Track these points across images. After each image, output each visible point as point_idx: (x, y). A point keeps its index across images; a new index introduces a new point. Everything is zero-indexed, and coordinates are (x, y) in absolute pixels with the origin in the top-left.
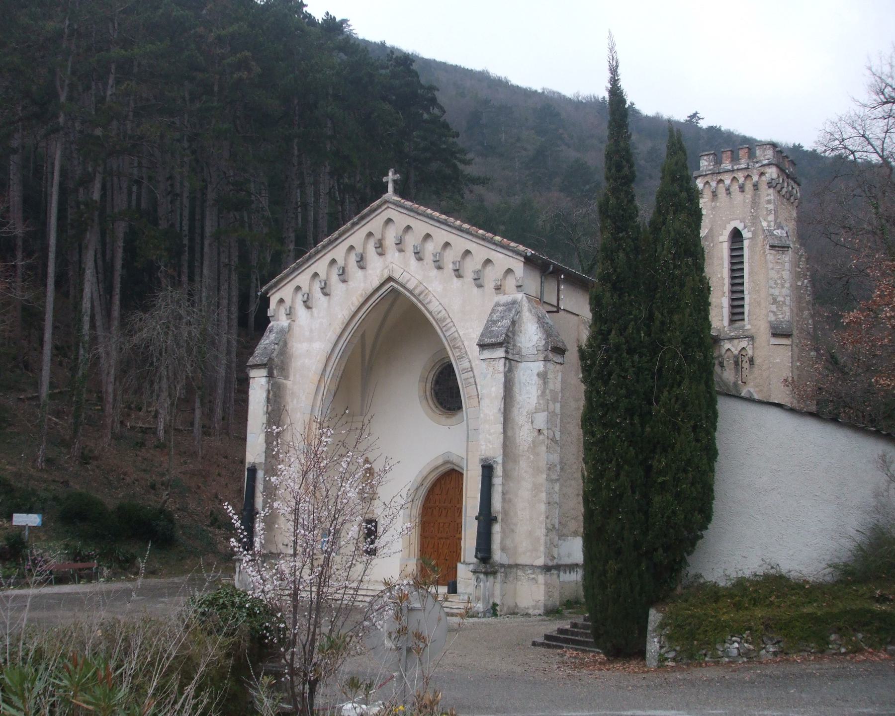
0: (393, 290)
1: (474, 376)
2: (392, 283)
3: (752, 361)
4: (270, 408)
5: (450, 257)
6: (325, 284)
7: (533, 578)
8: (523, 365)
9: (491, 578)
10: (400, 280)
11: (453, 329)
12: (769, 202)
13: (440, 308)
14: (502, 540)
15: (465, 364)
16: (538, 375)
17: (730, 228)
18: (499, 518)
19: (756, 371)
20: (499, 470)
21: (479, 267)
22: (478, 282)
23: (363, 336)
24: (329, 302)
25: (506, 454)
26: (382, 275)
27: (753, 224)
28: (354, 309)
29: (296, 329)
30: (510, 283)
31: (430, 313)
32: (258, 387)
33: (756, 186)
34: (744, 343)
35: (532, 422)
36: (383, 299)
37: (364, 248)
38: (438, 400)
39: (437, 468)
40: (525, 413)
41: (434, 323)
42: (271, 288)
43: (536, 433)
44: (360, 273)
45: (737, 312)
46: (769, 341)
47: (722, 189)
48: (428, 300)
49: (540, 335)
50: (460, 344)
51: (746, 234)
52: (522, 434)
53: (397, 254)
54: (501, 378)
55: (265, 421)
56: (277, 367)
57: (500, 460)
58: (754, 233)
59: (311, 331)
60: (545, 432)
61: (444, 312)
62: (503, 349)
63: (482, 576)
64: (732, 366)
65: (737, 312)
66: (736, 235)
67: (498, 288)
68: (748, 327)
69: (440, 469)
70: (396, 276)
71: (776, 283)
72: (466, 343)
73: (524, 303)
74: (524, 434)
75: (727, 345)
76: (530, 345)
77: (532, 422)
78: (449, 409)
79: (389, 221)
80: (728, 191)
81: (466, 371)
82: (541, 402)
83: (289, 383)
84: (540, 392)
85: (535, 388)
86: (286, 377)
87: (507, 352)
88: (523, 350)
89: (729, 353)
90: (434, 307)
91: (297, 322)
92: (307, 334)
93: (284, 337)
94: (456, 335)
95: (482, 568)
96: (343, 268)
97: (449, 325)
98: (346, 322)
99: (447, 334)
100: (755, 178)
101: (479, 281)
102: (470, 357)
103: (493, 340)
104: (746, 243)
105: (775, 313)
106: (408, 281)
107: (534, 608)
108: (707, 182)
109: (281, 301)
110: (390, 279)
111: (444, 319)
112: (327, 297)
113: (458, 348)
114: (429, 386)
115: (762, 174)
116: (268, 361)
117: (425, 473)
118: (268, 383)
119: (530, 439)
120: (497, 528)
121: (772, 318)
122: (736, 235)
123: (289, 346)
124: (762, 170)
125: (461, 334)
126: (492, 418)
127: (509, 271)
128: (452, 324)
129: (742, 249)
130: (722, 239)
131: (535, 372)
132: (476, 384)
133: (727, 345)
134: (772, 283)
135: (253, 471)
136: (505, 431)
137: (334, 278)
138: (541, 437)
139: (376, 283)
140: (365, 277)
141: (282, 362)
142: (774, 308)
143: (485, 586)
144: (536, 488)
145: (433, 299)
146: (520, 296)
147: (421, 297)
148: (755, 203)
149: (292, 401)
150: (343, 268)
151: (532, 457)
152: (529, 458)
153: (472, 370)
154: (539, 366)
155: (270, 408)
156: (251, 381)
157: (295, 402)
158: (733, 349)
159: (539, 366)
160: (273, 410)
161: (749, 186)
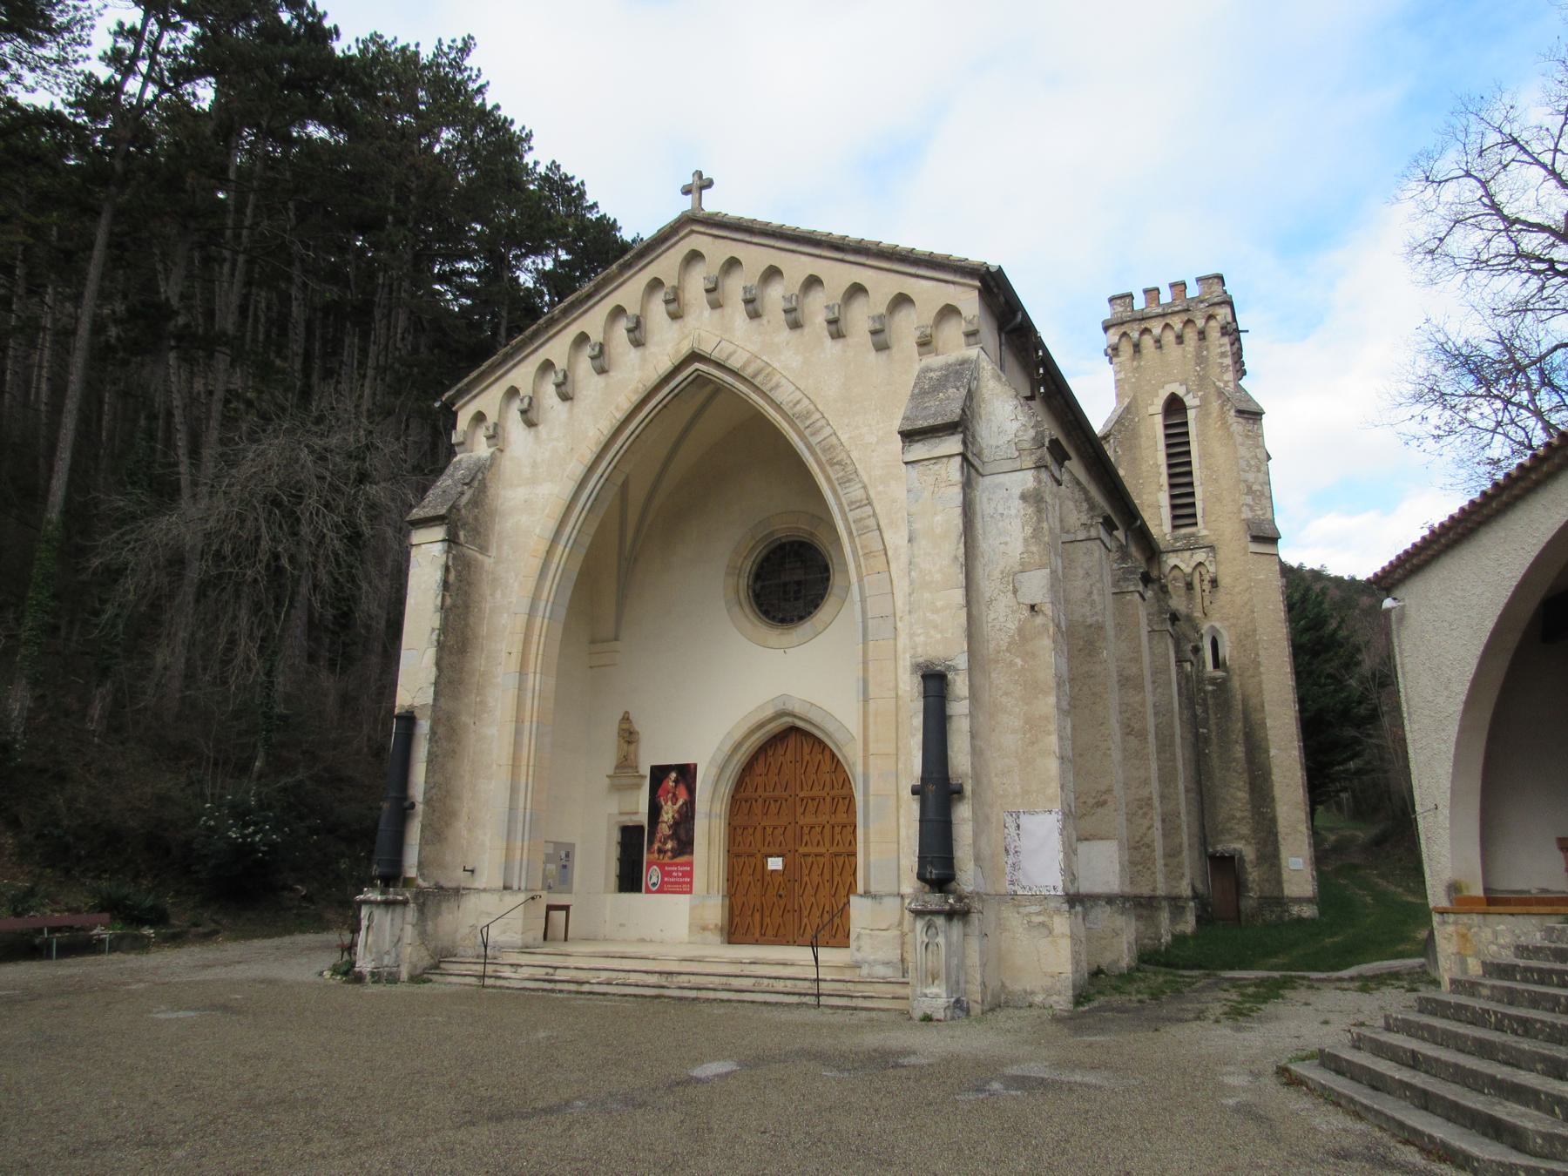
0: (700, 380)
1: (874, 514)
2: (697, 365)
3: (1214, 582)
4: (448, 601)
5: (817, 307)
6: (565, 376)
7: (1042, 924)
8: (987, 480)
9: (956, 928)
10: (715, 355)
11: (827, 432)
12: (1223, 355)
13: (798, 395)
14: (976, 835)
15: (856, 493)
16: (1023, 497)
17: (1164, 395)
18: (968, 789)
19: (1222, 597)
20: (960, 685)
21: (882, 309)
22: (881, 340)
23: (625, 486)
24: (571, 410)
25: (971, 653)
26: (677, 351)
27: (1201, 386)
28: (620, 416)
29: (507, 464)
30: (952, 333)
31: (778, 407)
32: (427, 559)
33: (1202, 335)
34: (1200, 556)
35: (1015, 592)
36: (677, 396)
37: (643, 308)
38: (760, 606)
39: (761, 726)
40: (997, 574)
41: (784, 426)
42: (460, 394)
43: (1026, 613)
44: (633, 354)
45: (1183, 510)
46: (1245, 548)
47: (1147, 341)
48: (772, 383)
49: (1022, 419)
50: (843, 456)
51: (1189, 401)
52: (993, 616)
53: (707, 312)
54: (956, 494)
55: (437, 624)
56: (465, 527)
57: (962, 662)
58: (1204, 400)
59: (534, 465)
60: (1048, 609)
61: (806, 402)
62: (959, 437)
63: (940, 921)
64: (1183, 592)
65: (1183, 510)
66: (1174, 406)
67: (925, 344)
68: (1204, 532)
69: (743, 749)
70: (707, 348)
71: (1249, 465)
72: (854, 455)
73: (984, 364)
74: (1002, 616)
75: (1172, 560)
76: (1003, 440)
77: (1015, 592)
78: (783, 621)
79: (694, 256)
80: (1158, 342)
81: (856, 505)
82: (1034, 549)
83: (488, 562)
84: (1029, 531)
85: (1017, 523)
86: (483, 549)
87: (965, 443)
88: (986, 452)
89: (1176, 572)
90: (784, 395)
91: (507, 454)
92: (527, 471)
93: (480, 479)
94: (834, 440)
95: (934, 900)
96: (601, 346)
97: (818, 424)
98: (604, 440)
99: (814, 440)
100: (1200, 323)
101: (881, 337)
102: (865, 478)
103: (931, 422)
104: (1191, 414)
105: (1252, 509)
106: (730, 355)
107: (1049, 992)
108: (1125, 334)
109: (480, 417)
110: (694, 356)
111: (808, 414)
112: (568, 404)
113: (839, 463)
114: (743, 583)
115: (1211, 317)
116: (450, 510)
117: (737, 736)
118: (448, 552)
119: (1012, 626)
120: (963, 813)
121: (1246, 514)
122: (1174, 406)
123: (491, 492)
124: (1211, 311)
125: (844, 438)
126: (938, 577)
127: (949, 311)
128: (823, 422)
129: (1185, 424)
130: (1151, 410)
131: (1017, 492)
132: (879, 529)
133: (1172, 560)
134: (1243, 464)
135: (409, 719)
136: (969, 603)
137: (584, 365)
138: (1039, 620)
139: (665, 365)
140: (644, 360)
141: (476, 518)
142: (1249, 499)
143: (949, 944)
144: (1032, 725)
145: (784, 381)
146: (973, 352)
147: (757, 382)
148: (1201, 360)
149: (492, 595)
150: (601, 346)
151: (1019, 661)
152: (1012, 664)
153: (870, 504)
154: (1027, 480)
155: (448, 601)
156: (414, 552)
157: (498, 594)
158: (1182, 566)
159: (1027, 480)
160: (454, 606)
161: (1191, 335)
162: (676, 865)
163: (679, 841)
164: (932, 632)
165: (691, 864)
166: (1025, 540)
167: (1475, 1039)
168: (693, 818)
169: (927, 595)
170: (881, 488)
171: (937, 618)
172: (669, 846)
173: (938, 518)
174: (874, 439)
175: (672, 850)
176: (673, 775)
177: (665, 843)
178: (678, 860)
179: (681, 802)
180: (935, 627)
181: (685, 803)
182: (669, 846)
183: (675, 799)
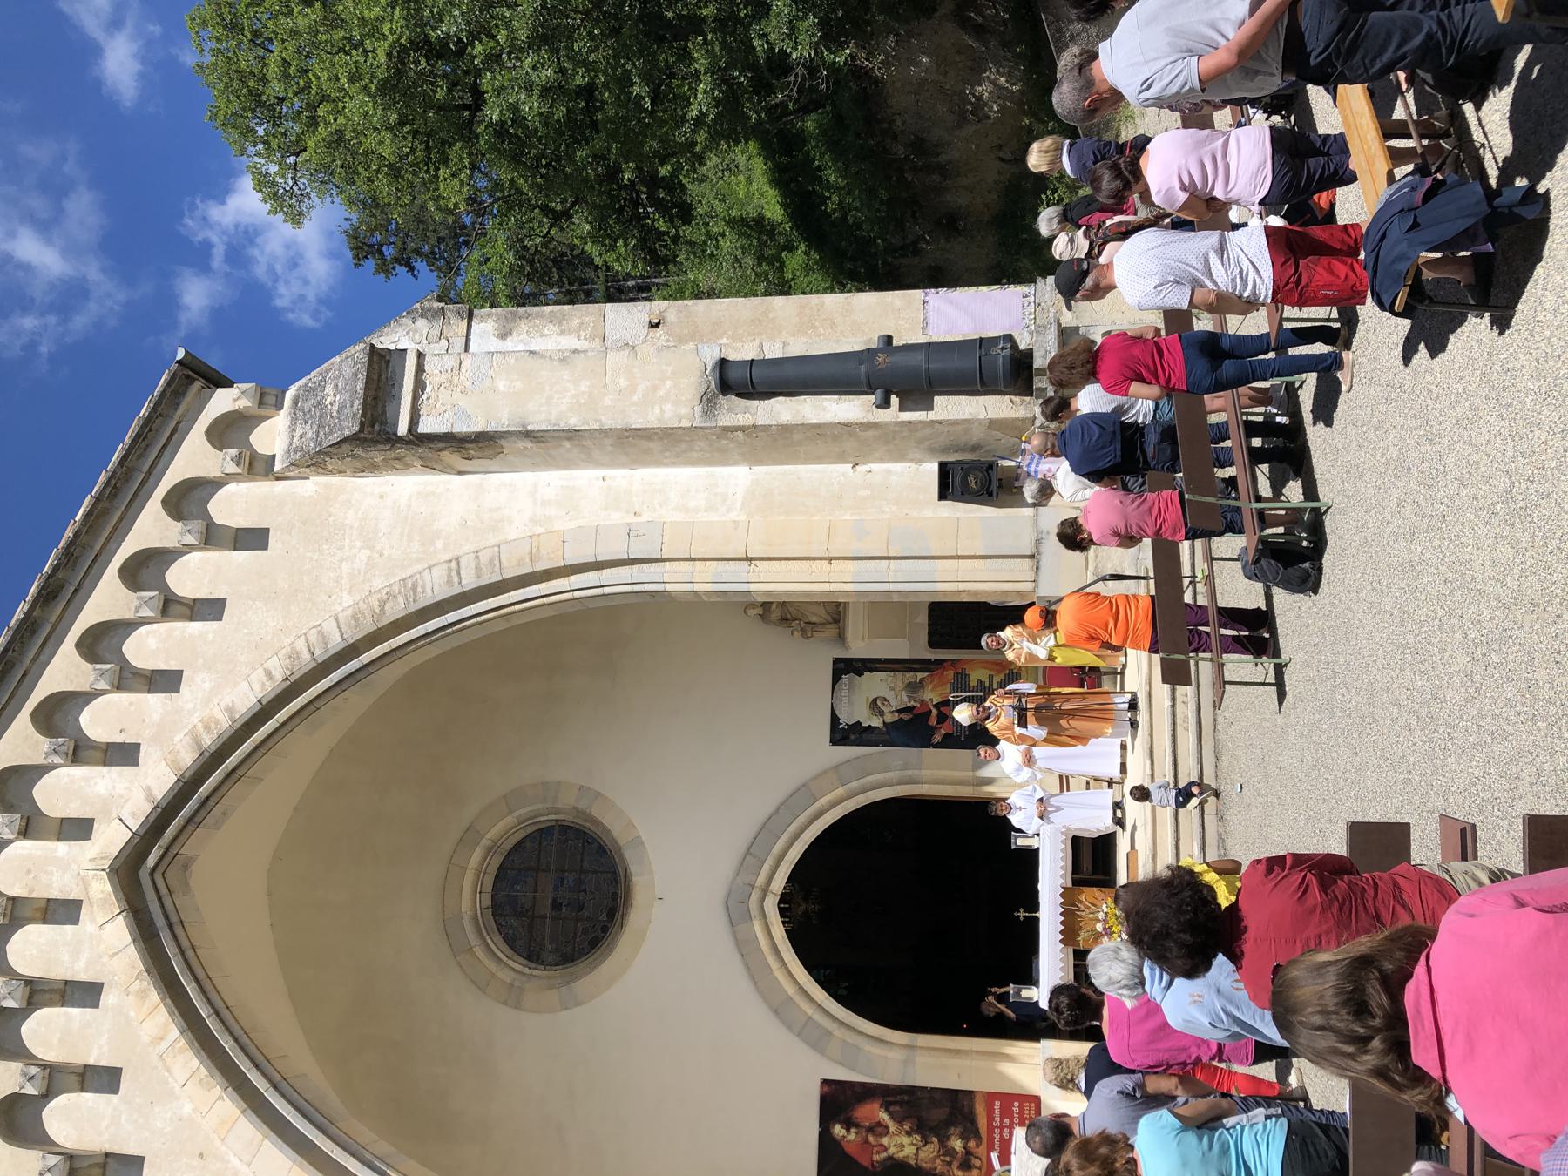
43: (659, 332)
126: (584, 386)
162: (991, 1129)
163: (950, 1122)
164: (662, 393)
165: (991, 1097)
166: (561, 333)
167: (1035, 922)
168: (911, 1090)
169: (607, 401)
170: (439, 544)
171: (641, 388)
172: (957, 1144)
173: (501, 385)
174: (365, 553)
175: (964, 1137)
176: (838, 1130)
177: (951, 1153)
178: (982, 1123)
179: (884, 1117)
180: (655, 388)
181: (887, 1107)
182: (957, 1144)
183: (878, 1129)
